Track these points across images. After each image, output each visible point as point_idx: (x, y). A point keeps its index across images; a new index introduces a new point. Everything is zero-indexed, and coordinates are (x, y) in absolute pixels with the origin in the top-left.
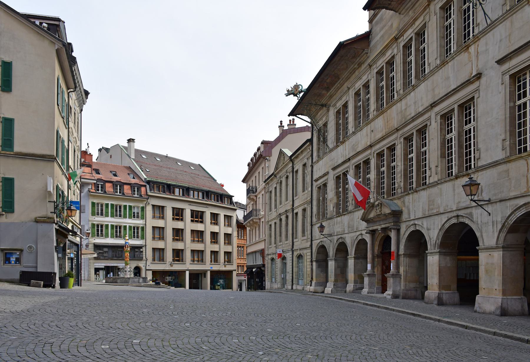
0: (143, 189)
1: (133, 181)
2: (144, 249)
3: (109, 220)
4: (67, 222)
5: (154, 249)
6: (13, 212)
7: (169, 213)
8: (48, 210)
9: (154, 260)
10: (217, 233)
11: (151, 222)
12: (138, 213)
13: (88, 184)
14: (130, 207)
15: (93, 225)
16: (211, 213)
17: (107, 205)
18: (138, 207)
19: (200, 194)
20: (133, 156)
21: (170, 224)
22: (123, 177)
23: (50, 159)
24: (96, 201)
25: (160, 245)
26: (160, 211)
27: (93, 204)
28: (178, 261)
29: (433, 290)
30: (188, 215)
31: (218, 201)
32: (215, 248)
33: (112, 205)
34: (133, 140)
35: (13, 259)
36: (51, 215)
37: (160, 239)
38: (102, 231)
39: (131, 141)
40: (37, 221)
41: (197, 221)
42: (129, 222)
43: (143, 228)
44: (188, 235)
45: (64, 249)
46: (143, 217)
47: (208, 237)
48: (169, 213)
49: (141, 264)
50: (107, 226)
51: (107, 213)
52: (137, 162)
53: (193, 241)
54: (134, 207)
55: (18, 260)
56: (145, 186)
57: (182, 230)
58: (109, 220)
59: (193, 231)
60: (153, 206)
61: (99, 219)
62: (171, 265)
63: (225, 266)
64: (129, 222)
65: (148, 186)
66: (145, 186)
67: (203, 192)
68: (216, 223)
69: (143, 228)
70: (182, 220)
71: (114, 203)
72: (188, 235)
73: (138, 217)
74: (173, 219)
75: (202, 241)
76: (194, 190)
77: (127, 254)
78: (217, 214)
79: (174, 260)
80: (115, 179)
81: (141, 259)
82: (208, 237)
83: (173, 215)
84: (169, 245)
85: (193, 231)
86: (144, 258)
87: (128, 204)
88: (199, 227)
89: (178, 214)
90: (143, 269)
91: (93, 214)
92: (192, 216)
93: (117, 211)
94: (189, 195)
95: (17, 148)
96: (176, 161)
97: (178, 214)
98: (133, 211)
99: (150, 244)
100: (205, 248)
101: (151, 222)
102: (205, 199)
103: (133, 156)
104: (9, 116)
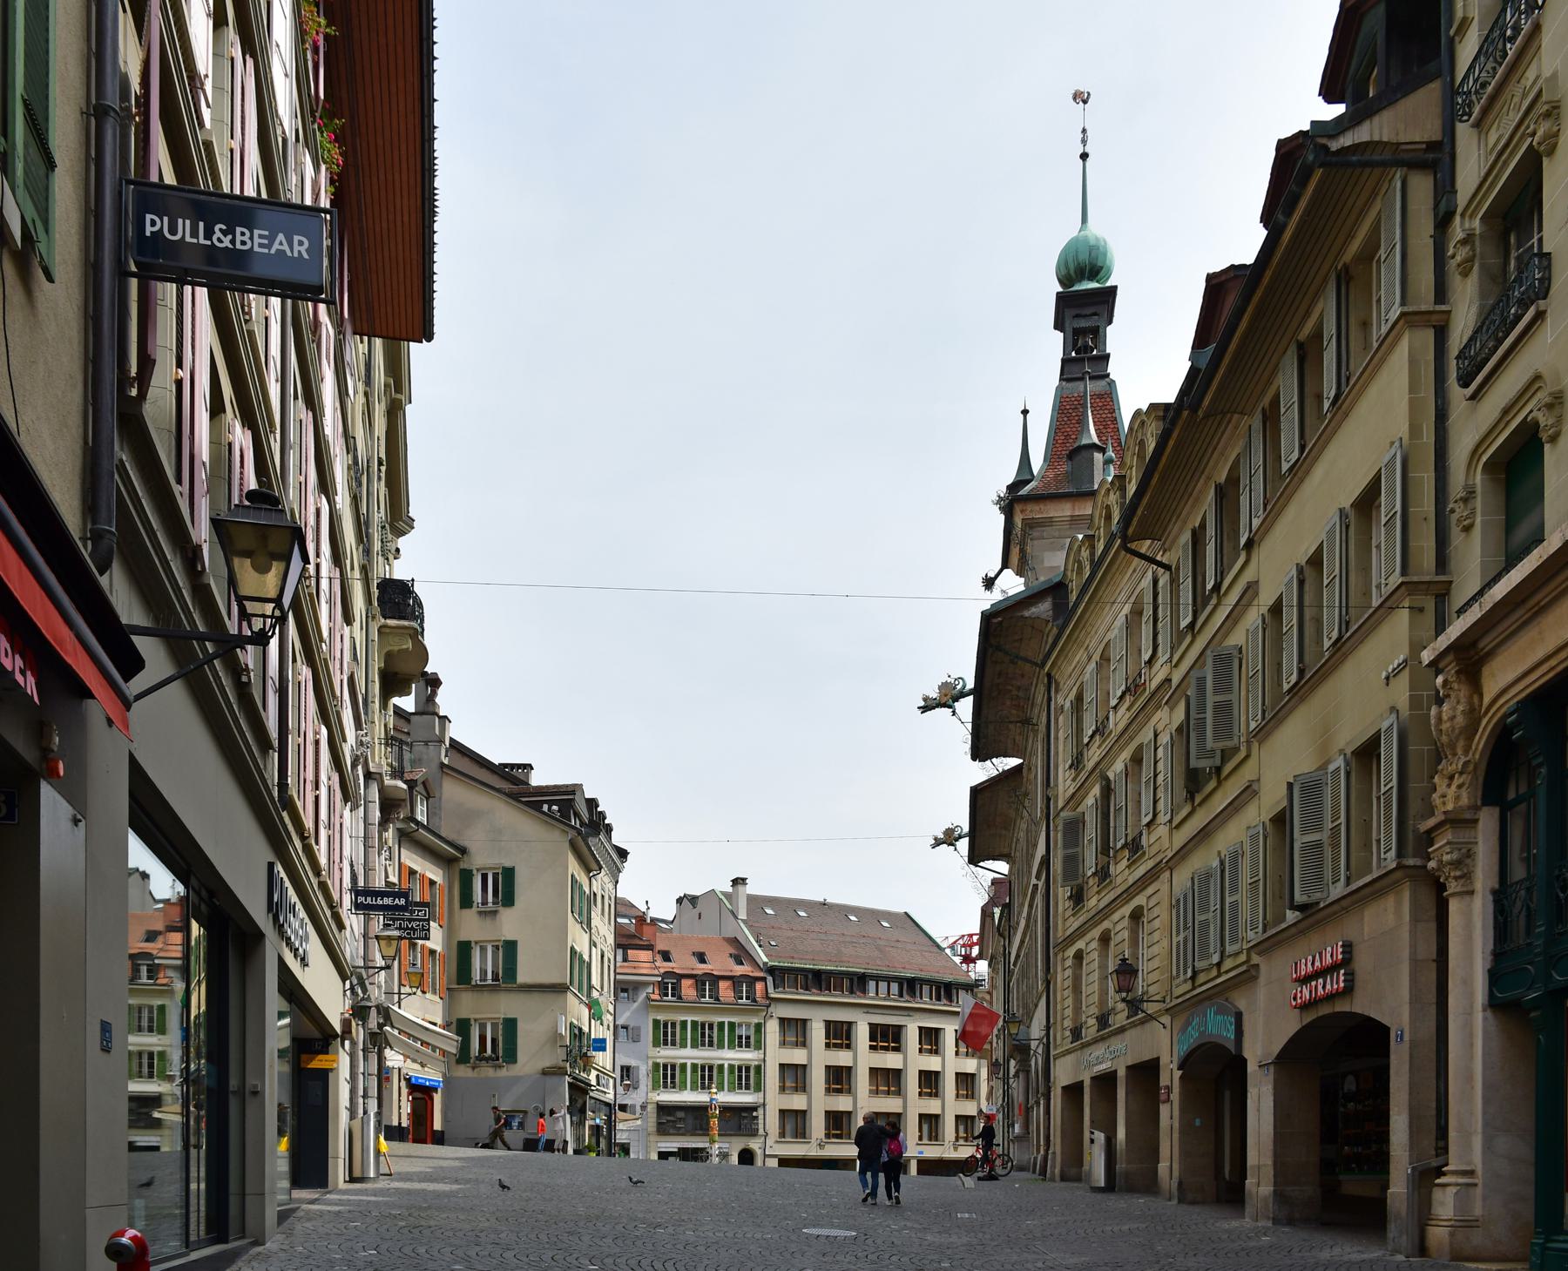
0: (759, 986)
1: (739, 970)
2: (761, 1111)
3: (689, 1055)
4: (586, 1069)
5: (782, 1112)
6: (515, 1062)
7: (817, 1033)
8: (556, 1057)
9: (782, 1134)
10: (937, 1073)
11: (775, 1053)
12: (748, 1038)
13: (646, 984)
14: (732, 1025)
15: (656, 1065)
16: (920, 1028)
17: (684, 1023)
18: (748, 1025)
19: (895, 987)
20: (742, 915)
21: (819, 1056)
22: (720, 963)
23: (560, 989)
24: (661, 1017)
25: (797, 1102)
26: (795, 1031)
27: (656, 1022)
28: (839, 1136)
29: (1168, 1166)
30: (862, 1034)
31: (938, 999)
32: (932, 1106)
33: (694, 1023)
34: (744, 880)
35: (515, 1124)
36: (562, 1064)
37: (796, 1089)
38: (673, 1076)
39: (738, 882)
40: (545, 1073)
41: (886, 1049)
42: (730, 1056)
43: (758, 1068)
44: (862, 1081)
45: (583, 1111)
46: (759, 1045)
47: (912, 1083)
48: (817, 1033)
49: (755, 1145)
50: (683, 1066)
51: (683, 1039)
52: (750, 927)
53: (875, 1092)
54: (740, 1025)
55: (521, 1125)
56: (764, 979)
57: (849, 1069)
58: (689, 1055)
59: (874, 1072)
60: (782, 1021)
61: (667, 1054)
62: (821, 1146)
63: (956, 1149)
64: (730, 1056)
65: (770, 979)
66: (764, 979)
67: (901, 981)
68: (935, 1051)
69: (758, 1068)
70: (848, 1047)
71: (699, 1018)
72: (862, 1081)
73: (748, 1046)
74: (828, 1045)
75: (898, 1093)
76: (878, 978)
77: (714, 1122)
78: (937, 1031)
79: (828, 1136)
80: (701, 969)
81: (753, 1133)
82: (912, 1083)
83: (828, 1037)
84: (818, 1101)
85: (874, 1072)
86: (761, 1131)
87: (726, 1020)
88: (891, 1060)
89: (839, 1035)
90: (759, 1152)
91: (656, 1044)
92: (872, 1038)
93: (704, 1035)
94: (864, 991)
95: (522, 977)
96: (845, 910)
97: (839, 1035)
98: (737, 1032)
99: (773, 1100)
100: (905, 1107)
101: (775, 1053)
102: (906, 997)
103: (742, 915)
104: (509, 938)
